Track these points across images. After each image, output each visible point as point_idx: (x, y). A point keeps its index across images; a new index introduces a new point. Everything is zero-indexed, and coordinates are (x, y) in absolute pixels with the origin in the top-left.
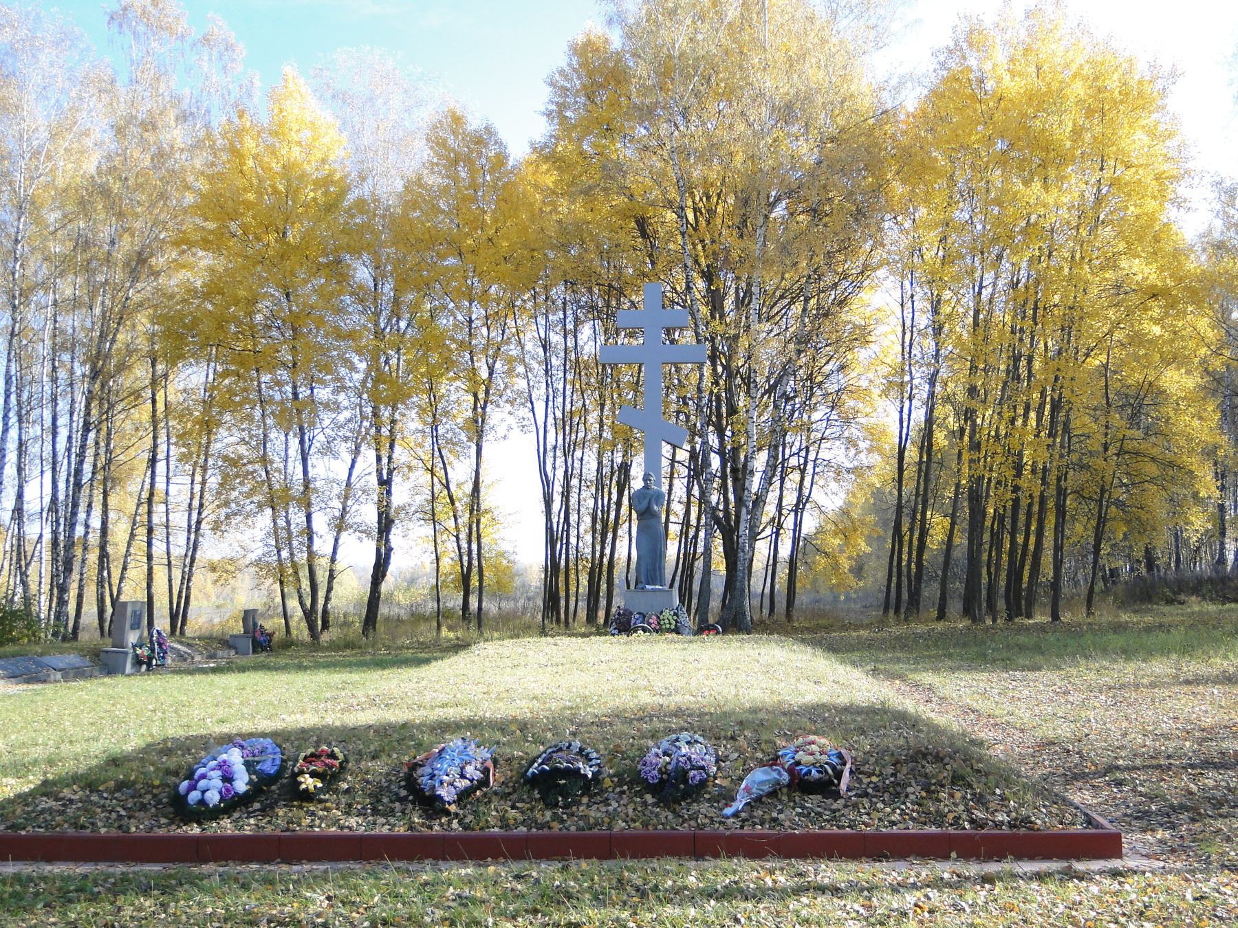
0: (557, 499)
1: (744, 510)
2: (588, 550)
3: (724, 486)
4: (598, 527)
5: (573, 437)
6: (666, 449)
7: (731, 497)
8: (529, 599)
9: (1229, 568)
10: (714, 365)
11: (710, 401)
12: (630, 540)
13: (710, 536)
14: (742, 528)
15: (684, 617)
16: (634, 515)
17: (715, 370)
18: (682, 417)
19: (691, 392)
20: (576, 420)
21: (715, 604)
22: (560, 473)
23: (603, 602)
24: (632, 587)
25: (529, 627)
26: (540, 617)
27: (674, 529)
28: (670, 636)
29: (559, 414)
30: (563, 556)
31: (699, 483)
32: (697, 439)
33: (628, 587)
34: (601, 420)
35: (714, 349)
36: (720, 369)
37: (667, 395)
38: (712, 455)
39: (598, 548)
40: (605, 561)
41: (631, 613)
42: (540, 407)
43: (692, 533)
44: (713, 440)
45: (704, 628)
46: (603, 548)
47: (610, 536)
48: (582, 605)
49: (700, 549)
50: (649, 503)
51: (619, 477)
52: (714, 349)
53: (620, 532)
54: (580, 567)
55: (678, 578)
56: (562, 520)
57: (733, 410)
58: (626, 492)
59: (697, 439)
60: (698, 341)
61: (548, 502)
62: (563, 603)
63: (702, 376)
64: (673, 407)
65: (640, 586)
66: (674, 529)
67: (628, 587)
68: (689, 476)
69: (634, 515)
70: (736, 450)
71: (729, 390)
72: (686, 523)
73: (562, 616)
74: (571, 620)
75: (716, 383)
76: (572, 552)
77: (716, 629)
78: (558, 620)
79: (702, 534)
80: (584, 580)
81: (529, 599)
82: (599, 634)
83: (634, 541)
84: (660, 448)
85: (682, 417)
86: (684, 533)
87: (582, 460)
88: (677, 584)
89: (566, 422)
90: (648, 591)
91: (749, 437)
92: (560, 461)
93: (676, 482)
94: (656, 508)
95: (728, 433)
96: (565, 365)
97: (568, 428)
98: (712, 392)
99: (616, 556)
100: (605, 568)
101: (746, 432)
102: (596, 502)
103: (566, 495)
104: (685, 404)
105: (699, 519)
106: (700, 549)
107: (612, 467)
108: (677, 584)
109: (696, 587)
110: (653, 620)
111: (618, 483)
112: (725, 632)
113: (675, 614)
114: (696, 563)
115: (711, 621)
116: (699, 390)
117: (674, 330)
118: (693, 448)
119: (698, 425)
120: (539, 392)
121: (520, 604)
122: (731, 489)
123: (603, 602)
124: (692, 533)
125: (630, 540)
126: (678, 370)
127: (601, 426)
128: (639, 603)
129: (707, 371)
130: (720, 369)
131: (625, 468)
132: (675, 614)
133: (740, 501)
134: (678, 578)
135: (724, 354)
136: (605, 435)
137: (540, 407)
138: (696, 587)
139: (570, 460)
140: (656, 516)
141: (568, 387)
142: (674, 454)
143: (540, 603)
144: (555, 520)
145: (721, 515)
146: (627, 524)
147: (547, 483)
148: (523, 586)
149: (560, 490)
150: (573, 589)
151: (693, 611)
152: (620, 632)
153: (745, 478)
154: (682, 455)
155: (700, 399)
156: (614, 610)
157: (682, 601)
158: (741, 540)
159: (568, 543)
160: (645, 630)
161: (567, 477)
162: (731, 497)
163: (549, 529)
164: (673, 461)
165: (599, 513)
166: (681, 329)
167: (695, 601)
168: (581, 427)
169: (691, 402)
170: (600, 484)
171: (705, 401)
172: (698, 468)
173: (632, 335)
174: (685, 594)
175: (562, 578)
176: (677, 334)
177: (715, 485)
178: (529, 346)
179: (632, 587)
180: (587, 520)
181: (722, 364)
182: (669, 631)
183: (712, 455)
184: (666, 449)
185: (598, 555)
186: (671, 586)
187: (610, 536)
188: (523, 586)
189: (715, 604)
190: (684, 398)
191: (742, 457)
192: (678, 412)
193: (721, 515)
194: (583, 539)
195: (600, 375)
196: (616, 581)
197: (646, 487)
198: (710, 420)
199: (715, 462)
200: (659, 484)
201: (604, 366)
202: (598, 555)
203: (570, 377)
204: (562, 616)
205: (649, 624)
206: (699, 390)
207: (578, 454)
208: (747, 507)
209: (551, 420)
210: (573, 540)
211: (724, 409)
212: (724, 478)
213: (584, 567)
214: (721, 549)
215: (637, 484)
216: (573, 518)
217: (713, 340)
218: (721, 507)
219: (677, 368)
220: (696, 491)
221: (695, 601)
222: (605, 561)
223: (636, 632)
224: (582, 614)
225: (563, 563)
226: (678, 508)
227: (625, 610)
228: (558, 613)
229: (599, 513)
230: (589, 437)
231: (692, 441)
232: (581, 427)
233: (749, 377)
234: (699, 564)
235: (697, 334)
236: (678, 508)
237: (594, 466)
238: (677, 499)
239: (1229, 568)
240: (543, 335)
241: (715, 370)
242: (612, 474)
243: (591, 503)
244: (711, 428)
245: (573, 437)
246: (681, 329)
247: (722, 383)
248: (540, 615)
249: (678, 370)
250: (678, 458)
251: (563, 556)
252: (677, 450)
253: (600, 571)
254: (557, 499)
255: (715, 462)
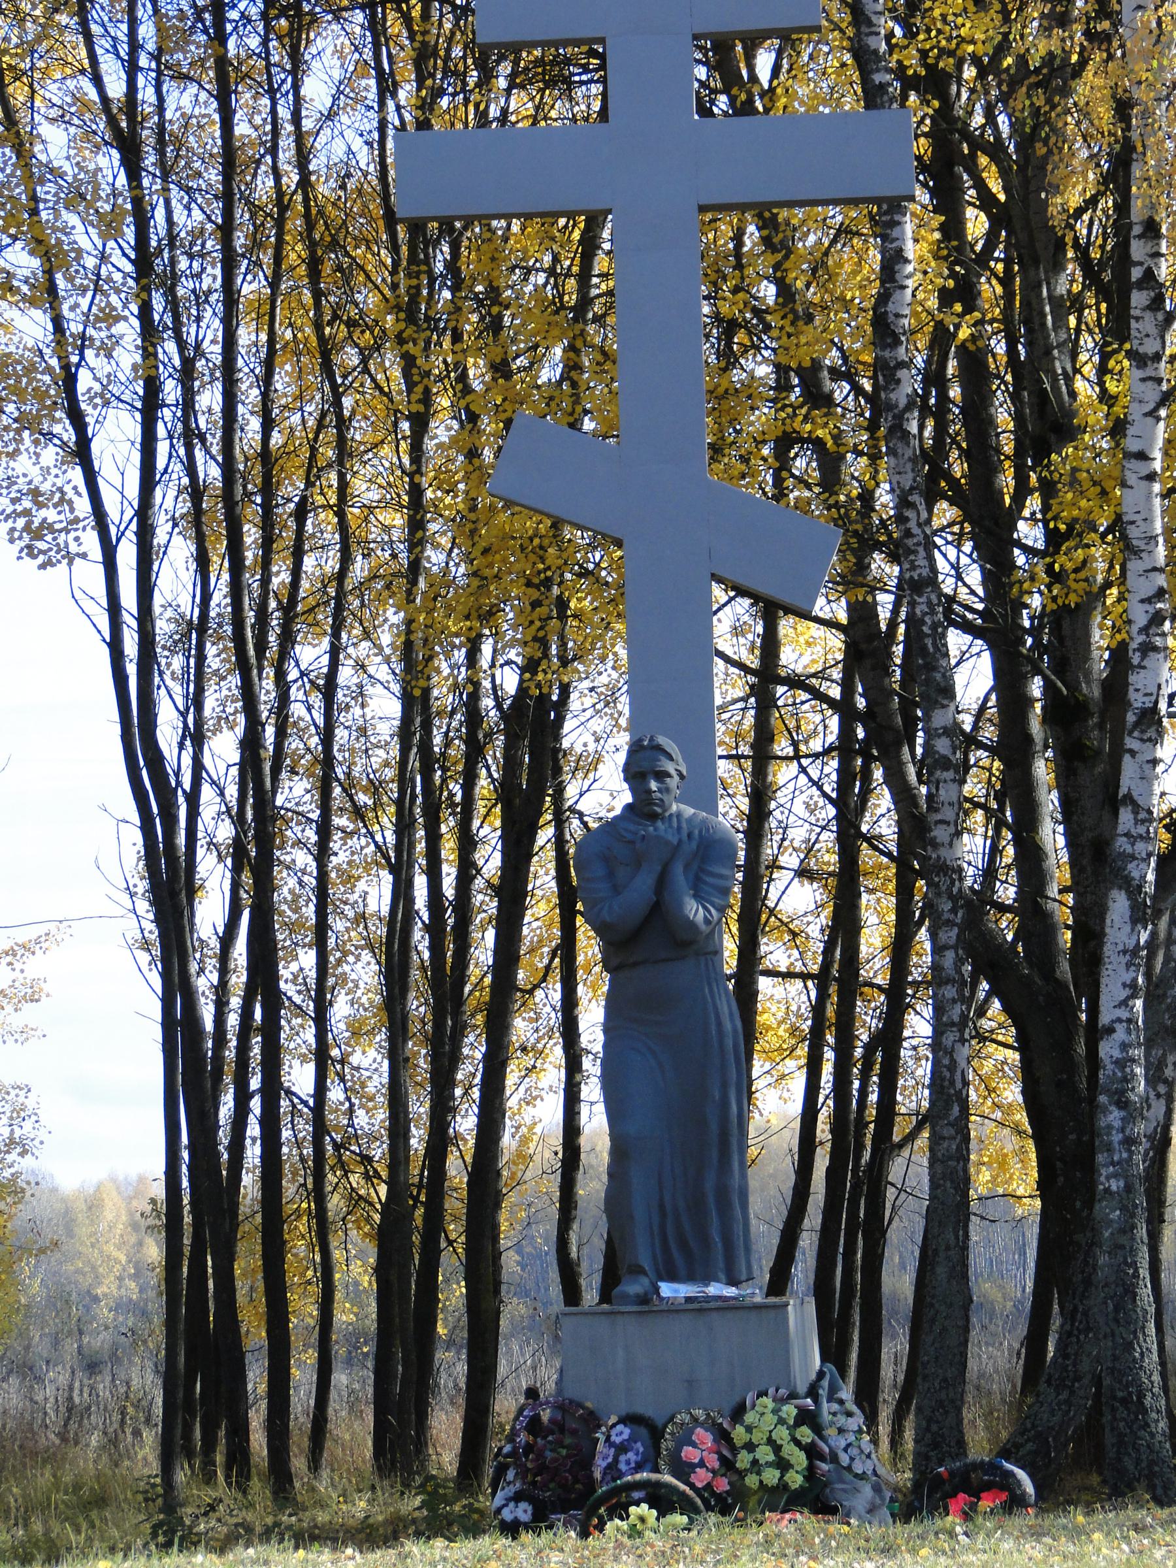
0: (214, 880)
1: (1119, 905)
2: (371, 1120)
3: (1016, 790)
4: (418, 1007)
5: (281, 577)
6: (732, 625)
7: (1053, 837)
8: (92, 1367)
9: (1002, 197)
10: (948, 204)
11: (934, 378)
12: (573, 1065)
13: (953, 1032)
14: (1112, 987)
15: (844, 1423)
16: (588, 946)
17: (953, 229)
18: (802, 463)
19: (844, 337)
20: (291, 489)
21: (993, 1355)
22: (224, 750)
23: (452, 1367)
24: (590, 1296)
25: (100, 1501)
26: (146, 1453)
27: (782, 1002)
28: (785, 1526)
29: (210, 472)
30: (253, 1153)
31: (896, 780)
32: (882, 566)
33: (572, 1294)
34: (416, 492)
35: (947, 129)
36: (976, 224)
37: (728, 359)
38: (956, 640)
39: (419, 1107)
40: (456, 1170)
41: (593, 1420)
42: (116, 437)
43: (868, 1019)
44: (959, 571)
45: (941, 1486)
46: (442, 1110)
47: (474, 1049)
48: (352, 1382)
49: (914, 1093)
50: (662, 882)
51: (510, 763)
52: (947, 129)
53: (521, 1028)
54: (335, 1203)
55: (808, 1242)
56: (239, 979)
57: (1047, 426)
58: (545, 835)
59: (882, 566)
60: (873, 96)
61: (169, 887)
62: (257, 1380)
63: (893, 260)
64: (760, 418)
65: (633, 1287)
66: (782, 1002)
67: (572, 1294)
68: (844, 748)
69: (588, 946)
70: (1067, 623)
71: (1026, 321)
72: (838, 975)
73: (258, 1440)
74: (298, 1463)
75: (962, 293)
76: (294, 1133)
77: (1007, 1483)
78: (239, 1456)
79: (919, 1026)
80: (357, 1267)
81: (92, 1367)
82: (436, 1525)
83: (591, 1067)
84: (709, 613)
85: (802, 463)
86: (830, 1023)
87: (329, 688)
88: (803, 1270)
89: (239, 508)
90: (673, 1309)
91: (1129, 549)
92: (221, 696)
93: (783, 774)
94: (694, 911)
95: (1029, 533)
96: (226, 230)
97: (251, 535)
98: (941, 338)
99: (508, 1141)
100: (455, 1204)
101: (1118, 524)
102: (402, 891)
103: (255, 857)
104: (818, 399)
105: (900, 948)
106: (914, 1093)
107: (474, 717)
108: (803, 1270)
109: (899, 1280)
110: (701, 1448)
111: (506, 792)
112: (1054, 1495)
113: (806, 1417)
114: (896, 1169)
115: (979, 1444)
116: (884, 330)
117: (752, 43)
118: (862, 613)
119: (884, 497)
120: (112, 364)
121: (47, 1394)
122: (1050, 801)
123: (452, 1367)
124: (868, 1019)
125: (573, 1065)
126: (777, 241)
127: (417, 512)
128: (631, 1368)
129: (917, 241)
130: (976, 224)
131: (535, 722)
132: (806, 1417)
133: (1096, 861)
134: (808, 1242)
135: (996, 151)
136: (434, 558)
137: (116, 437)
138: (899, 1280)
139: (267, 689)
140: (696, 946)
141: (245, 336)
142: (770, 645)
143: (145, 1381)
144: (205, 983)
145: (1007, 927)
146: (555, 992)
147: (158, 795)
148: (60, 1299)
149: (225, 832)
150: (303, 1310)
151: (888, 1397)
152: (540, 1520)
153: (1118, 751)
154: (810, 648)
155: (886, 372)
156: (506, 1405)
157: (833, 1353)
158: (1108, 1050)
159: (273, 1088)
160: (663, 1502)
161: (257, 769)
162: (1053, 837)
163: (179, 1026)
164: (766, 675)
165: (420, 940)
166: (788, 39)
167: (895, 1349)
168: (322, 525)
169: (840, 391)
170: (421, 801)
171: (910, 383)
172: (886, 700)
173: (554, 76)
174: (848, 1315)
175: (247, 1264)
176: (764, 61)
177: (974, 787)
178: (55, 143)
179: (590, 1296)
180: (364, 972)
181: (986, 201)
182: (782, 1500)
183: (956, 640)
184: (732, 625)
185: (418, 1139)
186: (779, 1282)
187: (474, 1049)
188: (60, 1299)
189: (993, 1355)
190: (810, 375)
191: (1100, 639)
192: (785, 443)
193: (1007, 927)
194: (344, 1065)
195: (404, 277)
196: (510, 1262)
197: (643, 809)
198: (939, 472)
199: (974, 677)
200: (705, 791)
201: (417, 227)
202: (418, 1139)
203: (251, 287)
204: (258, 1440)
205: (682, 1470)
206: (884, 330)
207: (311, 654)
208: (1134, 890)
209: (169, 499)
210: (300, 1077)
211: (1003, 417)
212: (1014, 750)
213: (355, 1200)
214: (1012, 1093)
215: (600, 794)
216: (298, 966)
217: (935, 83)
218: (1007, 893)
219: (768, 224)
220: (881, 817)
221: (895, 1349)
222: (456, 1170)
223: (620, 1510)
224: (354, 1432)
225: (250, 1182)
226: (797, 900)
227: (565, 1406)
228: (240, 1430)
229: (420, 940)
230: (360, 568)
231: (856, 579)
232: (322, 525)
233: (1121, 257)
234: (911, 1170)
235: (864, 59)
236: (797, 900)
237: (385, 707)
238: (791, 860)
239: (1002, 197)
240: (116, 88)
241: (953, 229)
242: (475, 752)
243: (377, 893)
244: (945, 513)
245: (281, 577)
246: (788, 39)
247: (989, 289)
248: (151, 1436)
249: (777, 241)
250: (791, 658)
251: (253, 1153)
252: (786, 626)
253: (433, 1219)
254: (214, 880)
255: (974, 677)
